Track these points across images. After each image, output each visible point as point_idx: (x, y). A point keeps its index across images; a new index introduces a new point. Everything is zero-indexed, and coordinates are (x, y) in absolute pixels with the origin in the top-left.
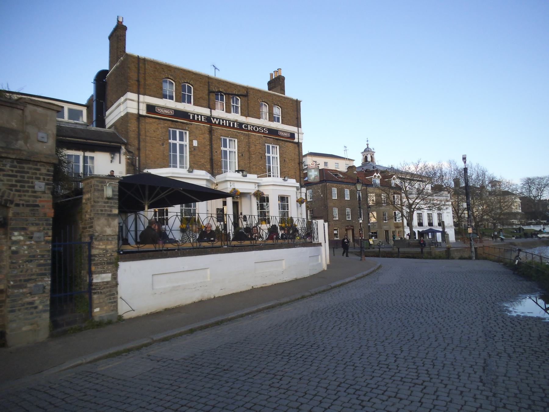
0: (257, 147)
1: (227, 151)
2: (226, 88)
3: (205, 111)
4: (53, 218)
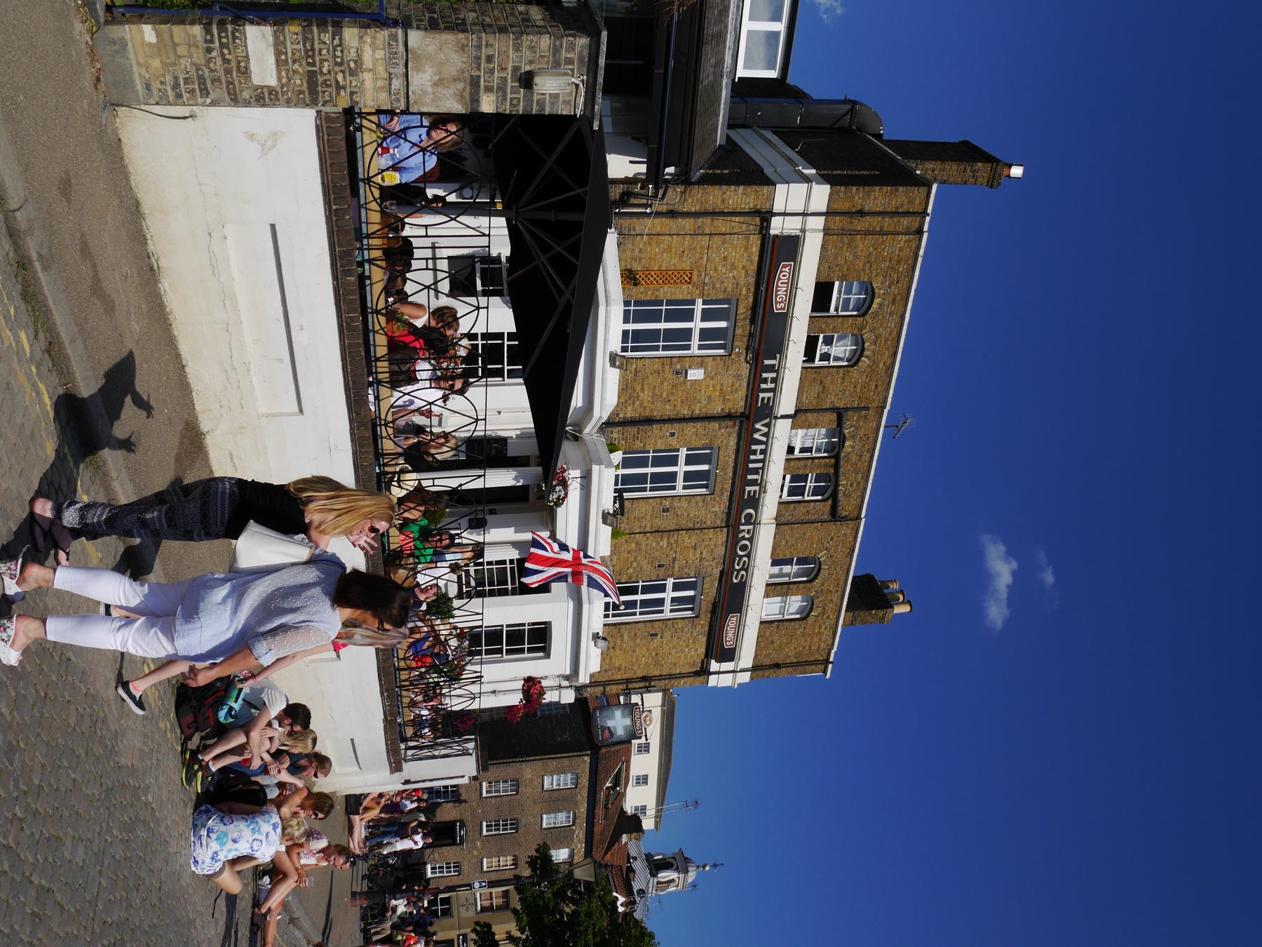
0: (692, 551)
1: (677, 465)
2: (854, 458)
3: (787, 402)
4: (558, 703)
